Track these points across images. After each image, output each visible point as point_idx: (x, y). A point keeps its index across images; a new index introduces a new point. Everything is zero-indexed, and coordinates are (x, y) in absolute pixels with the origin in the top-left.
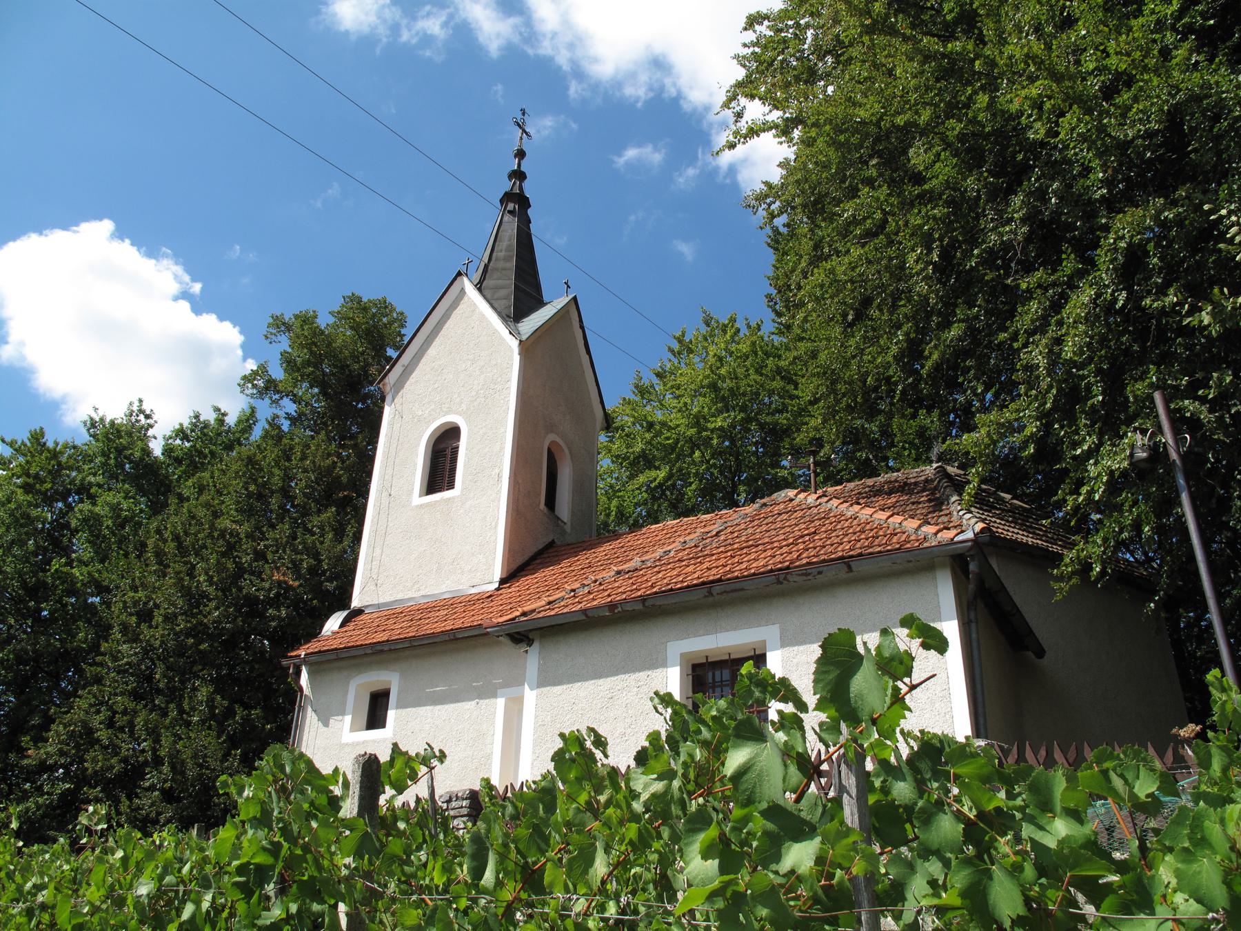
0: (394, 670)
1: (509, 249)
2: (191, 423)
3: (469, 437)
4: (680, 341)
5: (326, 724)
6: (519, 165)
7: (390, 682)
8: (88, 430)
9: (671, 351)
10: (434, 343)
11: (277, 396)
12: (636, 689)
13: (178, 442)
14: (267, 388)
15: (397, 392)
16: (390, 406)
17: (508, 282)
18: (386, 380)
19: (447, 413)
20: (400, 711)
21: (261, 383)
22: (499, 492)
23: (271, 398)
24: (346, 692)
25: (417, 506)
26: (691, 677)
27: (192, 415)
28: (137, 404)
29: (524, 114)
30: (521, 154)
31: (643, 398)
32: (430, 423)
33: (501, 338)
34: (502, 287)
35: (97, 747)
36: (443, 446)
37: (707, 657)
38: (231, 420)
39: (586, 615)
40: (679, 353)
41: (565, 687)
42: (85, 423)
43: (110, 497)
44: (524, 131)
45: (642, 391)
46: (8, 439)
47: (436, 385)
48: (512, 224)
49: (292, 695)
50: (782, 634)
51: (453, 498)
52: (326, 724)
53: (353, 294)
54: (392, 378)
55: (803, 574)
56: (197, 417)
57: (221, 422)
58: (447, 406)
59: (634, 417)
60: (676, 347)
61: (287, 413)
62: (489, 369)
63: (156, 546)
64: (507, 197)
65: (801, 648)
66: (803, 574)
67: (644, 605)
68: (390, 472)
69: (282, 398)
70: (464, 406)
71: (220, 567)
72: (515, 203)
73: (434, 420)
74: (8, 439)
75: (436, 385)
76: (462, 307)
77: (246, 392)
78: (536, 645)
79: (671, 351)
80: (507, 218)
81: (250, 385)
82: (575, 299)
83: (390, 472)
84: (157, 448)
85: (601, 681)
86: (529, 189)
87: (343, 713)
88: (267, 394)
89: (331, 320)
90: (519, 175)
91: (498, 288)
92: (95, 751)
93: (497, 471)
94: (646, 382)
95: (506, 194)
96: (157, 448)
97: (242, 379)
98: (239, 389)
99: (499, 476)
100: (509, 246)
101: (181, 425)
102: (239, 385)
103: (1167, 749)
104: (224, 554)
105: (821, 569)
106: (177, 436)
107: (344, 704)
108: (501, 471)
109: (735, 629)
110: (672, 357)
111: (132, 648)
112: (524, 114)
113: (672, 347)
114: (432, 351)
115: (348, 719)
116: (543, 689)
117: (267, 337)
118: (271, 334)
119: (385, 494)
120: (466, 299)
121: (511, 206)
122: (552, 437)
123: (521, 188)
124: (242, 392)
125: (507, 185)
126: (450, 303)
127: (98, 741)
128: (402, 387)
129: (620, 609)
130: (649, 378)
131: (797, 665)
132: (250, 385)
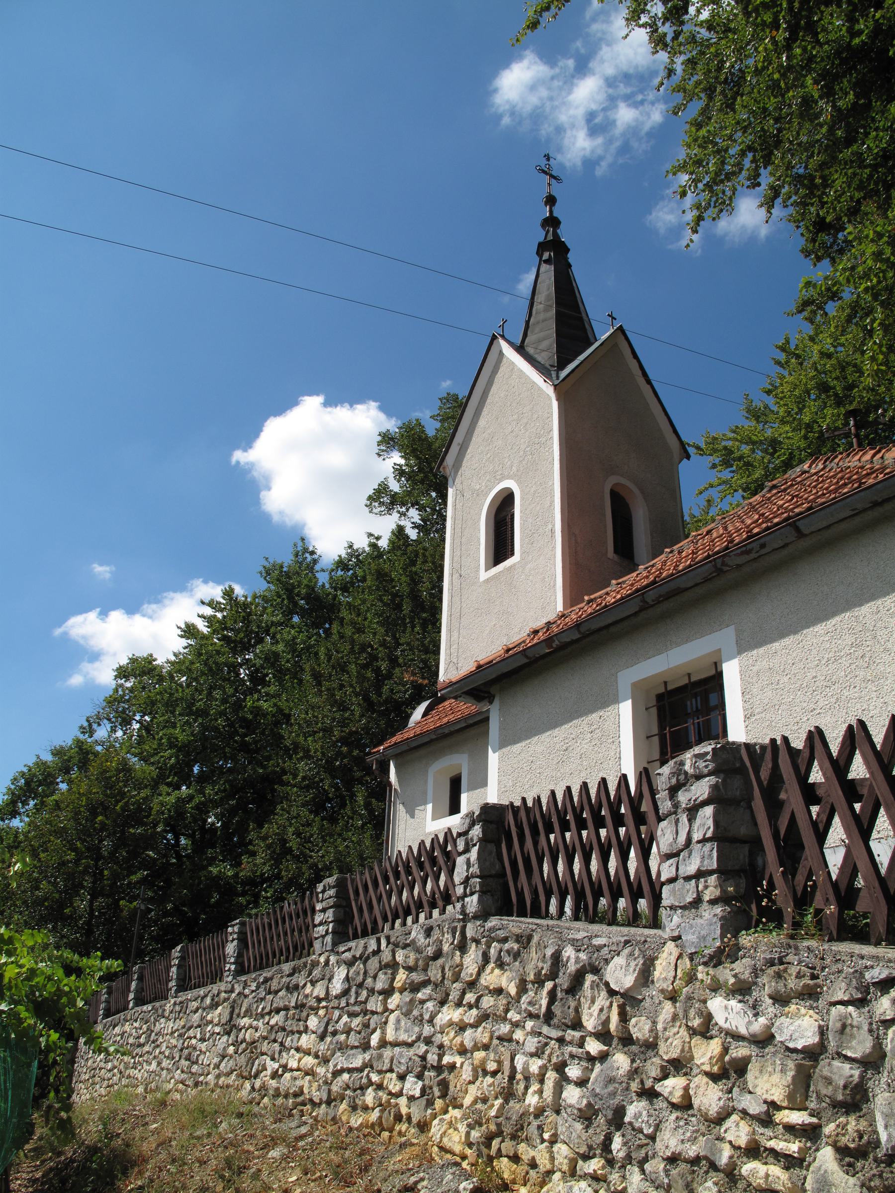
0: (463, 753)
1: (548, 298)
2: (348, 554)
3: (522, 499)
4: (783, 349)
5: (412, 816)
6: (551, 212)
7: (460, 766)
8: (265, 578)
9: (778, 363)
10: (483, 413)
11: (404, 509)
12: (589, 735)
13: (340, 573)
14: (392, 503)
15: (456, 472)
16: (452, 487)
17: (549, 332)
18: (445, 463)
19: (501, 480)
20: (471, 793)
21: (386, 500)
22: (554, 548)
23: (398, 512)
24: (426, 782)
25: (484, 581)
26: (654, 711)
27: (346, 546)
28: (300, 544)
29: (548, 159)
30: (551, 200)
31: (758, 422)
32: (487, 494)
33: (540, 389)
34: (544, 339)
35: (288, 857)
36: (504, 514)
37: (665, 683)
38: (383, 543)
39: (527, 657)
40: (787, 362)
41: (523, 744)
42: (261, 573)
43: (288, 634)
44: (552, 176)
45: (757, 415)
46: (207, 601)
47: (489, 455)
48: (548, 272)
49: (382, 791)
50: (738, 636)
51: (514, 565)
52: (412, 816)
53: (448, 394)
54: (450, 460)
55: (743, 553)
56: (351, 547)
57: (374, 546)
58: (500, 472)
59: (737, 440)
60: (782, 357)
61: (413, 523)
62: (532, 425)
63: (313, 669)
64: (542, 247)
65: (761, 650)
66: (743, 553)
67: (580, 632)
68: (458, 553)
69: (408, 510)
70: (514, 469)
71: (362, 678)
72: (550, 251)
73: (491, 490)
74: (207, 601)
75: (489, 455)
76: (503, 369)
77: (375, 511)
78: (497, 702)
79: (778, 363)
80: (544, 267)
81: (376, 504)
82: (621, 329)
83: (458, 553)
84: (323, 579)
85: (556, 731)
86: (565, 236)
87: (425, 803)
88: (393, 509)
89: (438, 425)
90: (552, 222)
91: (540, 341)
92: (288, 861)
93: (550, 527)
94: (758, 404)
95: (541, 245)
96: (323, 579)
97: (368, 500)
98: (367, 509)
99: (552, 531)
100: (548, 296)
101: (340, 556)
102: (366, 506)
103: (419, 704)
104: (365, 666)
105: (762, 541)
106: (337, 568)
107: (425, 793)
108: (554, 526)
109: (687, 641)
110: (781, 370)
111: (307, 764)
112: (548, 159)
113: (777, 358)
114: (482, 423)
115: (430, 807)
116: (504, 750)
117: (379, 455)
118: (383, 451)
119: (456, 576)
120: (504, 360)
121: (546, 256)
122: (612, 481)
123: (555, 234)
124: (370, 512)
125: (540, 235)
126: (491, 369)
127: (290, 850)
128: (461, 466)
129: (557, 642)
130: (760, 400)
131: (758, 673)
132: (376, 504)
